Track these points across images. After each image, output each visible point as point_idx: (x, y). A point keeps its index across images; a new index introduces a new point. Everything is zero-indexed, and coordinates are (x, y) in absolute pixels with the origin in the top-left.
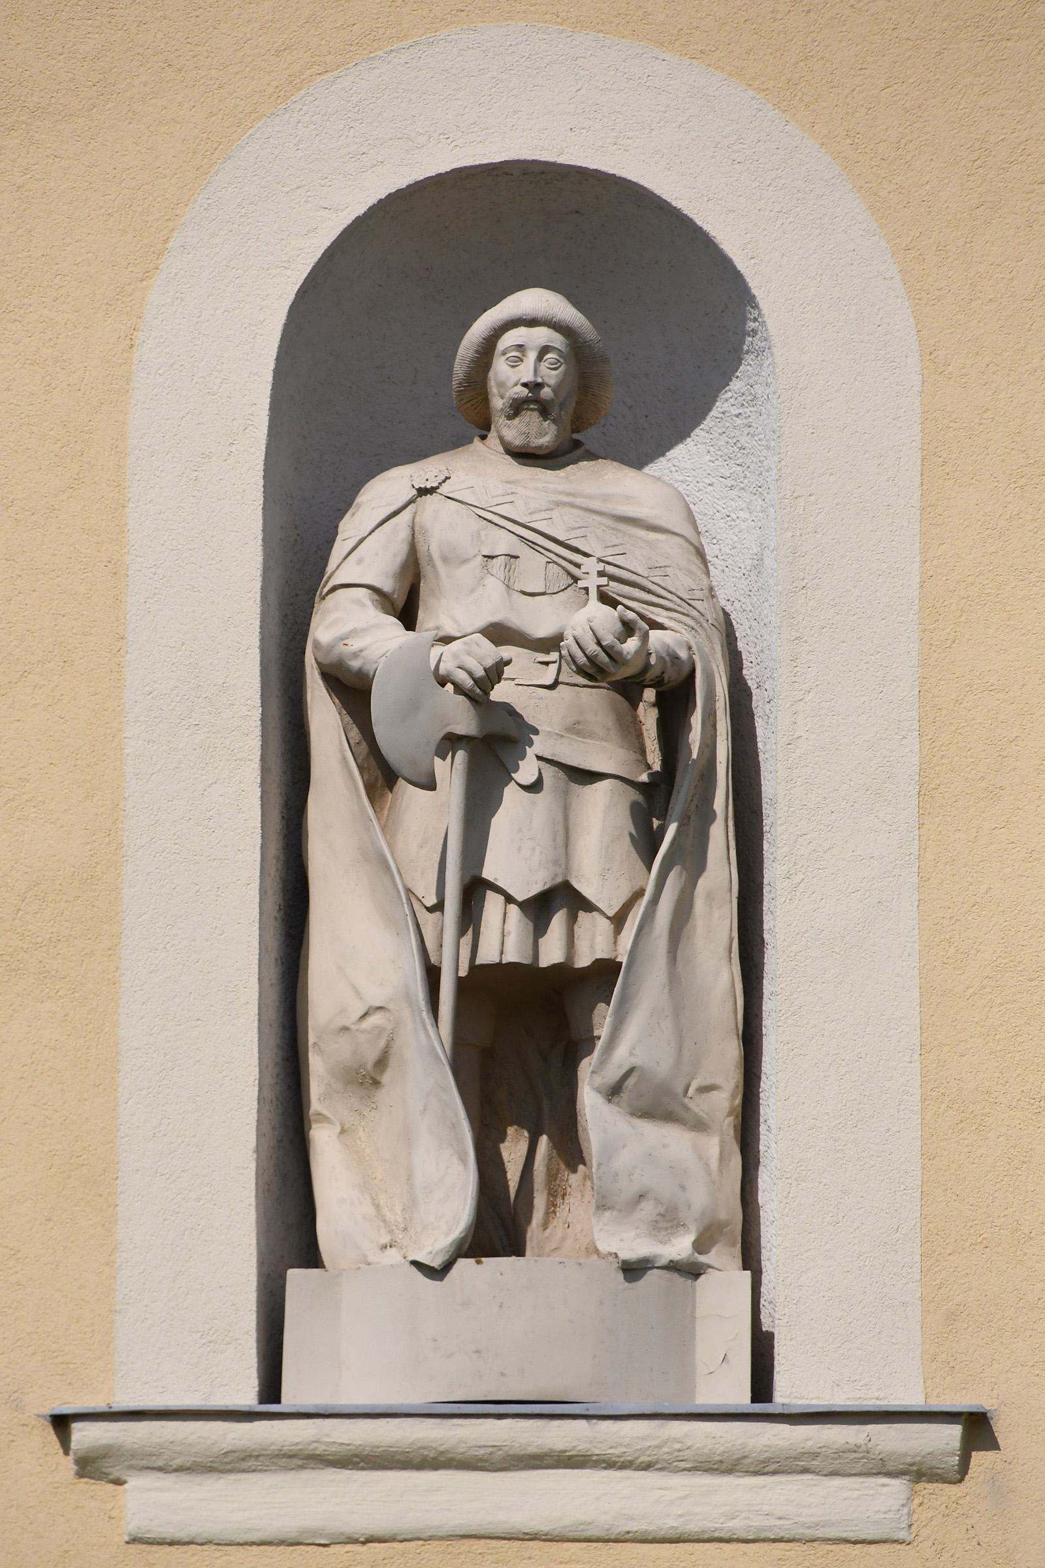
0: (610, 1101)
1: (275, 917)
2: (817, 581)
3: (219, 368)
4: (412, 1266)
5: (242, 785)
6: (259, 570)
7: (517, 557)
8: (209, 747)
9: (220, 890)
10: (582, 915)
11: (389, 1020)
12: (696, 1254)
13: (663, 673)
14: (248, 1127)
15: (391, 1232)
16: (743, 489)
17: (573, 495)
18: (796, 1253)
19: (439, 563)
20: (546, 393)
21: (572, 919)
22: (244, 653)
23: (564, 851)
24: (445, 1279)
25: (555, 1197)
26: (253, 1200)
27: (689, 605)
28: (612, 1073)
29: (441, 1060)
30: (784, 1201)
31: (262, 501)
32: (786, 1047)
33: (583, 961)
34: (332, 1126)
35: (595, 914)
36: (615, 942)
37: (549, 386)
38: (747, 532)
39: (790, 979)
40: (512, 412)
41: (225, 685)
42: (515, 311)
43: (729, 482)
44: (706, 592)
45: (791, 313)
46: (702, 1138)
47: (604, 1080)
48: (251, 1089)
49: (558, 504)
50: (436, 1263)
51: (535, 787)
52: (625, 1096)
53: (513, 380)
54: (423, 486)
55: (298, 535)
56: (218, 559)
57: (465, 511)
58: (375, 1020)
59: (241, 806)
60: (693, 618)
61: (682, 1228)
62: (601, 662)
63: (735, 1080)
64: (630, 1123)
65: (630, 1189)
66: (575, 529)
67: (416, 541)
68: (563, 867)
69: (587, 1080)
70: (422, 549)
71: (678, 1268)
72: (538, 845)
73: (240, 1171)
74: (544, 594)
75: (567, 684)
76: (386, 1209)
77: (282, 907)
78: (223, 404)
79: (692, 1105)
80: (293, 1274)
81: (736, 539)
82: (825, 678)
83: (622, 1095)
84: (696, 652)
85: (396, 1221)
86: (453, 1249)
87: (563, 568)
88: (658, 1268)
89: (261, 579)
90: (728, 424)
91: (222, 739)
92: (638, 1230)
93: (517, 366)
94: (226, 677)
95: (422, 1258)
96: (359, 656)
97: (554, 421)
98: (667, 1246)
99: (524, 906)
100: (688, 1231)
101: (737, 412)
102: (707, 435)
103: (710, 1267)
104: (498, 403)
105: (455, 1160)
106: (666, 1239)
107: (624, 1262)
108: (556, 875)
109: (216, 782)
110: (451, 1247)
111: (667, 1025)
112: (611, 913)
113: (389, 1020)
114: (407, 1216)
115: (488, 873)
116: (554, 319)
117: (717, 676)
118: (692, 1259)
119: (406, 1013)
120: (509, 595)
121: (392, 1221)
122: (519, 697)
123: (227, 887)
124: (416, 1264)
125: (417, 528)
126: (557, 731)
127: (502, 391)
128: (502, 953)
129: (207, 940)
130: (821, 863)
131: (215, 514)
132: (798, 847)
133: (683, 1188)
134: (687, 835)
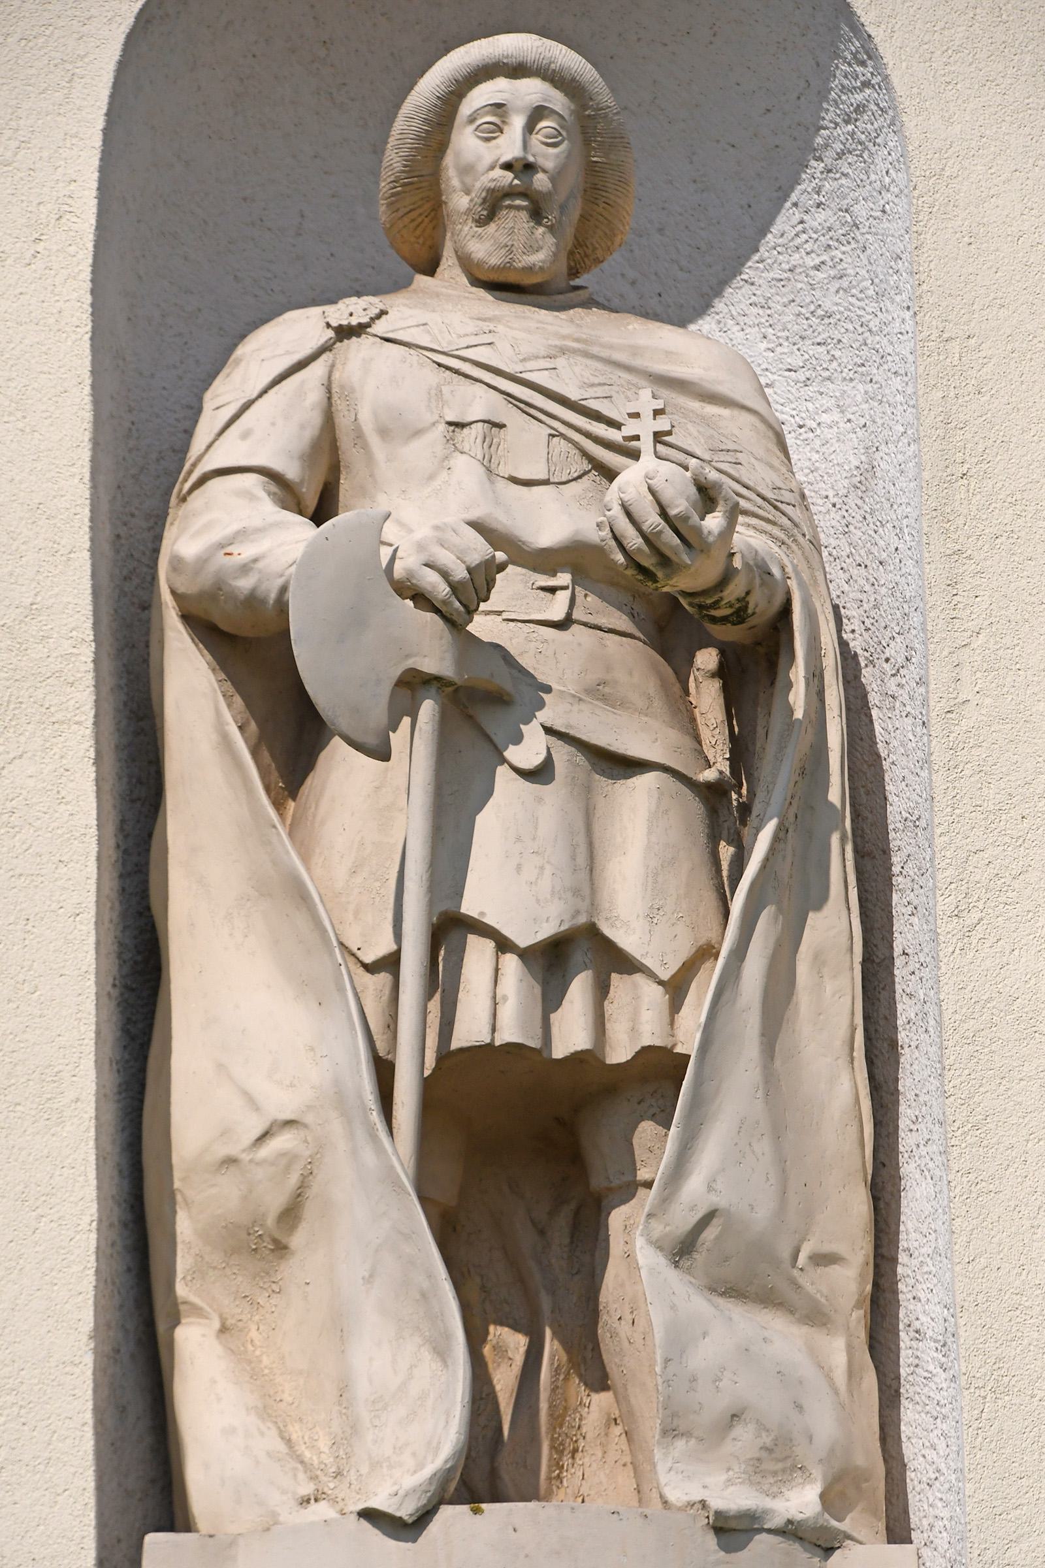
0: (676, 1264)
1: (109, 994)
2: (984, 466)
3: (13, 124)
4: (361, 1519)
5: (64, 761)
6: (87, 433)
7: (501, 426)
8: (9, 702)
9: (31, 924)
10: (617, 981)
11: (306, 1141)
12: (827, 1516)
13: (748, 593)
14: (81, 1298)
15: (314, 1478)
16: (829, 379)
17: (585, 342)
18: (998, 1511)
19: (374, 441)
20: (541, 181)
21: (602, 990)
22: (64, 558)
23: (588, 878)
24: (421, 1540)
25: (561, 1453)
26: (89, 1417)
27: (776, 507)
28: (681, 1218)
29: (402, 1187)
30: (976, 1425)
31: (89, 328)
32: (965, 1179)
33: (620, 1053)
34: (207, 1321)
35: (638, 978)
36: (672, 1023)
37: (545, 171)
38: (838, 441)
39: (967, 1072)
40: (485, 213)
41: (34, 607)
42: (491, 51)
43: (801, 376)
44: (797, 495)
45: (928, 64)
46: (819, 1337)
47: (668, 1229)
48: (85, 1236)
49: (563, 351)
50: (406, 1511)
51: (540, 774)
52: (699, 1257)
53: (488, 160)
54: (345, 322)
55: (133, 423)
56: (19, 415)
57: (415, 358)
58: (282, 1142)
59: (63, 793)
60: (782, 528)
61: (800, 1472)
62: (665, 544)
63: (864, 1252)
64: (709, 1300)
65: (715, 1404)
66: (593, 385)
67: (333, 409)
68: (588, 901)
69: (641, 1227)
70: (343, 421)
71: (800, 1534)
72: (548, 862)
73: (67, 1369)
74: (546, 482)
75: (585, 624)
76: (303, 1447)
77: (117, 982)
78: (22, 179)
79: (804, 1280)
80: (153, 1540)
81: (815, 457)
82: (1003, 612)
83: (695, 1255)
84: (792, 575)
85: (322, 1462)
86: (433, 1488)
87: (576, 445)
88: (769, 1531)
89: (90, 446)
90: (799, 285)
91: (31, 690)
92: (731, 1473)
93: (494, 138)
94: (36, 595)
95: (380, 1502)
96: (252, 569)
97: (551, 229)
98: (777, 1500)
99: (525, 955)
100: (809, 1479)
101: (817, 261)
102: (761, 311)
103: (849, 1537)
104: (460, 202)
105: (426, 1355)
106: (775, 1489)
107: (718, 1514)
108: (578, 912)
109: (21, 757)
110: (430, 1484)
111: (764, 1147)
112: (665, 975)
113: (306, 1141)
114: (341, 1453)
115: (470, 906)
116: (553, 66)
117: (821, 619)
118: (821, 1522)
119: (336, 1127)
120: (492, 482)
121: (316, 1462)
122: (511, 639)
123: (42, 919)
124: (370, 1515)
125: (335, 389)
126: (573, 692)
127: (468, 180)
128: (494, 1030)
129: (9, 1001)
130: (1009, 894)
131: (12, 345)
132: (971, 869)
133: (799, 1407)
134: (784, 857)
